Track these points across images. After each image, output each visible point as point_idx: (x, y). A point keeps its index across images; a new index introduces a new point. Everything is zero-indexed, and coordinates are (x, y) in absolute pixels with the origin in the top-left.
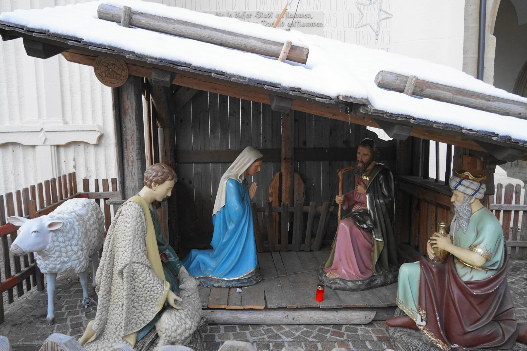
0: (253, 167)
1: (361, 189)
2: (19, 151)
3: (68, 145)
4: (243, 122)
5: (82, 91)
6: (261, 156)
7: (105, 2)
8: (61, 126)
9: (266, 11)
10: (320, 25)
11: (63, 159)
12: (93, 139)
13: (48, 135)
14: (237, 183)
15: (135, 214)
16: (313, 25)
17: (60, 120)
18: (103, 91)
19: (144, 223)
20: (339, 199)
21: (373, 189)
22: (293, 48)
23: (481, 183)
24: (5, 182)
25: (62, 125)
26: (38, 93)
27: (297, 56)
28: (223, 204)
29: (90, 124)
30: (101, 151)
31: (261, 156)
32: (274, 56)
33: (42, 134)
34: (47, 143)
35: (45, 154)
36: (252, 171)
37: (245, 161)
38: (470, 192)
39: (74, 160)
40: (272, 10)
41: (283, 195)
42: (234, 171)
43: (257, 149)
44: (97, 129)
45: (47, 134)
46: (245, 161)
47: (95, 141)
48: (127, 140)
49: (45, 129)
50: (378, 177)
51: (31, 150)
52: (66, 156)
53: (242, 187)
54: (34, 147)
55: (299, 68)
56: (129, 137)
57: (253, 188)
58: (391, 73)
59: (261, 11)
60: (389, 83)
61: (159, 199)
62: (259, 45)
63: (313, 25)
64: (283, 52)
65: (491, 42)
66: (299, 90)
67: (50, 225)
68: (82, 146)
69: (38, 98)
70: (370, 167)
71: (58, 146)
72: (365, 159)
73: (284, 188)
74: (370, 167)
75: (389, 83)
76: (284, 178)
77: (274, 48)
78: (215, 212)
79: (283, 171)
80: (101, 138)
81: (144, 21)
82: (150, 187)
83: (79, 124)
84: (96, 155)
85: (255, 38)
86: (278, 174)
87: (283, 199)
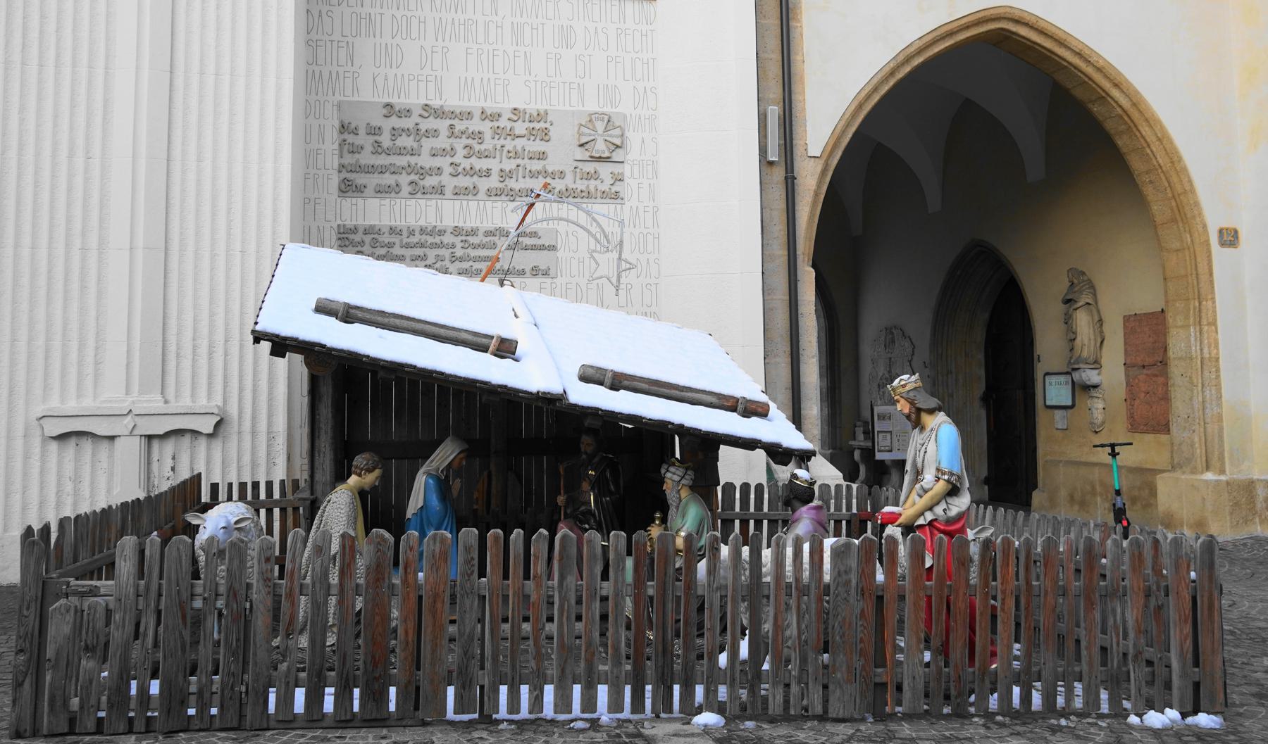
0: (457, 460)
1: (585, 486)
2: (87, 445)
3: (168, 434)
4: (439, 404)
5: (194, 354)
6: (466, 446)
7: (323, 296)
8: (156, 404)
9: (468, 225)
10: (553, 248)
11: (155, 456)
12: (207, 426)
13: (139, 420)
14: (438, 479)
15: (348, 500)
16: (542, 248)
17: (159, 397)
18: (271, 366)
19: (355, 510)
20: (561, 499)
21: (600, 486)
22: (503, 341)
23: (687, 469)
24: (58, 492)
25: (161, 404)
26: (128, 357)
27: (506, 349)
28: (420, 504)
29: (202, 403)
30: (217, 445)
31: (466, 446)
32: (484, 349)
33: (129, 417)
34: (135, 432)
35: (129, 449)
36: (455, 465)
37: (446, 454)
38: (677, 478)
39: (174, 458)
40: (478, 224)
41: (493, 501)
42: (434, 465)
43: (459, 436)
44: (216, 411)
45: (137, 419)
46: (446, 454)
47: (210, 430)
48: (320, 429)
49: (136, 412)
50: (604, 471)
51: (105, 445)
52: (160, 452)
53: (443, 484)
54: (112, 438)
55: (508, 362)
56: (322, 426)
57: (456, 485)
58: (592, 367)
59: (460, 225)
60: (590, 376)
61: (367, 488)
62: (470, 338)
63: (542, 248)
64: (493, 344)
65: (807, 277)
66: (505, 387)
67: (236, 523)
68: (188, 437)
69: (128, 365)
70: (596, 460)
71: (150, 438)
72: (590, 450)
73: (494, 491)
74: (596, 460)
75: (590, 376)
76: (494, 478)
77: (484, 341)
78: (409, 515)
79: (493, 468)
80: (218, 425)
81: (360, 314)
82: (360, 475)
83: (186, 403)
84: (209, 449)
85: (466, 331)
86: (485, 473)
87: (493, 506)
